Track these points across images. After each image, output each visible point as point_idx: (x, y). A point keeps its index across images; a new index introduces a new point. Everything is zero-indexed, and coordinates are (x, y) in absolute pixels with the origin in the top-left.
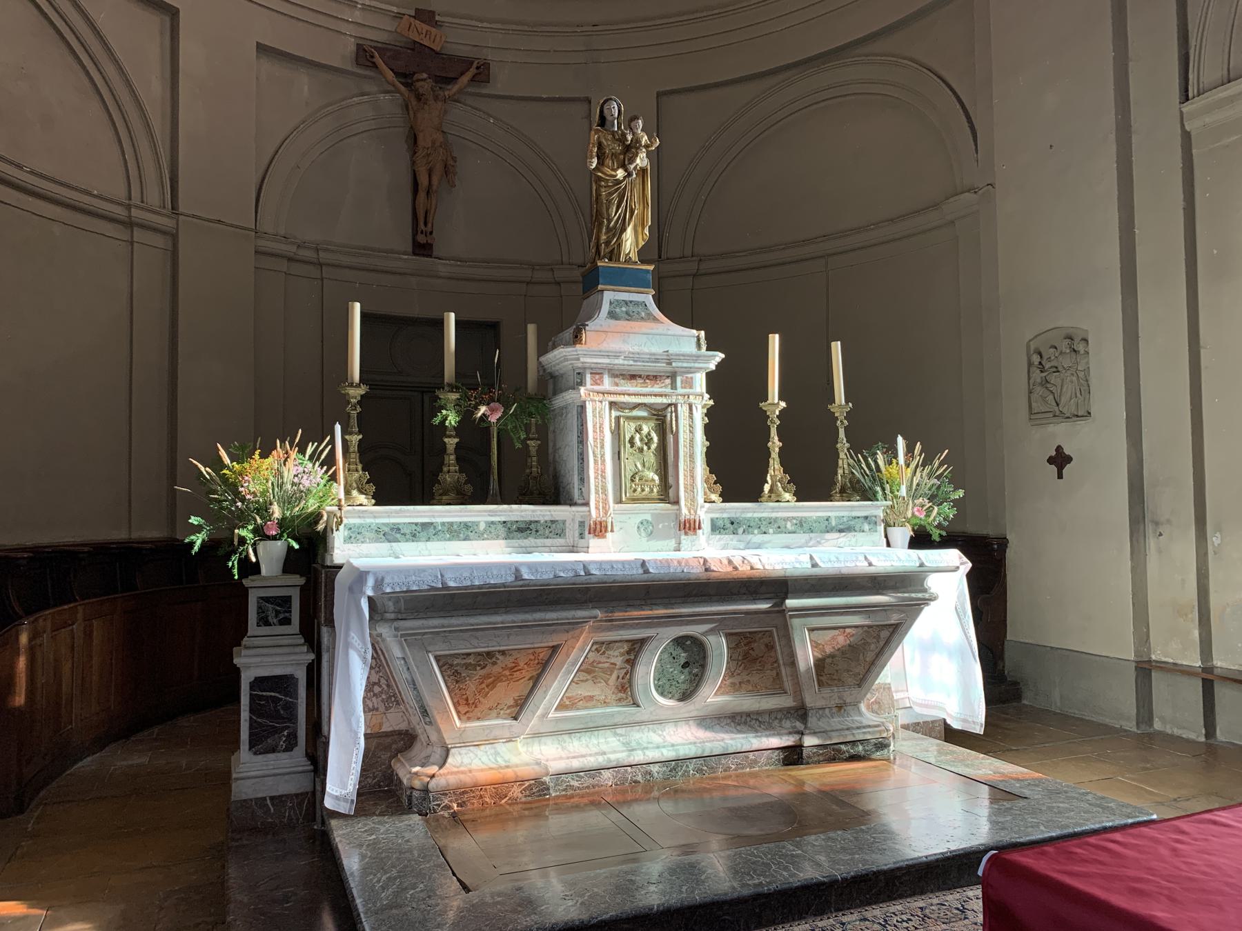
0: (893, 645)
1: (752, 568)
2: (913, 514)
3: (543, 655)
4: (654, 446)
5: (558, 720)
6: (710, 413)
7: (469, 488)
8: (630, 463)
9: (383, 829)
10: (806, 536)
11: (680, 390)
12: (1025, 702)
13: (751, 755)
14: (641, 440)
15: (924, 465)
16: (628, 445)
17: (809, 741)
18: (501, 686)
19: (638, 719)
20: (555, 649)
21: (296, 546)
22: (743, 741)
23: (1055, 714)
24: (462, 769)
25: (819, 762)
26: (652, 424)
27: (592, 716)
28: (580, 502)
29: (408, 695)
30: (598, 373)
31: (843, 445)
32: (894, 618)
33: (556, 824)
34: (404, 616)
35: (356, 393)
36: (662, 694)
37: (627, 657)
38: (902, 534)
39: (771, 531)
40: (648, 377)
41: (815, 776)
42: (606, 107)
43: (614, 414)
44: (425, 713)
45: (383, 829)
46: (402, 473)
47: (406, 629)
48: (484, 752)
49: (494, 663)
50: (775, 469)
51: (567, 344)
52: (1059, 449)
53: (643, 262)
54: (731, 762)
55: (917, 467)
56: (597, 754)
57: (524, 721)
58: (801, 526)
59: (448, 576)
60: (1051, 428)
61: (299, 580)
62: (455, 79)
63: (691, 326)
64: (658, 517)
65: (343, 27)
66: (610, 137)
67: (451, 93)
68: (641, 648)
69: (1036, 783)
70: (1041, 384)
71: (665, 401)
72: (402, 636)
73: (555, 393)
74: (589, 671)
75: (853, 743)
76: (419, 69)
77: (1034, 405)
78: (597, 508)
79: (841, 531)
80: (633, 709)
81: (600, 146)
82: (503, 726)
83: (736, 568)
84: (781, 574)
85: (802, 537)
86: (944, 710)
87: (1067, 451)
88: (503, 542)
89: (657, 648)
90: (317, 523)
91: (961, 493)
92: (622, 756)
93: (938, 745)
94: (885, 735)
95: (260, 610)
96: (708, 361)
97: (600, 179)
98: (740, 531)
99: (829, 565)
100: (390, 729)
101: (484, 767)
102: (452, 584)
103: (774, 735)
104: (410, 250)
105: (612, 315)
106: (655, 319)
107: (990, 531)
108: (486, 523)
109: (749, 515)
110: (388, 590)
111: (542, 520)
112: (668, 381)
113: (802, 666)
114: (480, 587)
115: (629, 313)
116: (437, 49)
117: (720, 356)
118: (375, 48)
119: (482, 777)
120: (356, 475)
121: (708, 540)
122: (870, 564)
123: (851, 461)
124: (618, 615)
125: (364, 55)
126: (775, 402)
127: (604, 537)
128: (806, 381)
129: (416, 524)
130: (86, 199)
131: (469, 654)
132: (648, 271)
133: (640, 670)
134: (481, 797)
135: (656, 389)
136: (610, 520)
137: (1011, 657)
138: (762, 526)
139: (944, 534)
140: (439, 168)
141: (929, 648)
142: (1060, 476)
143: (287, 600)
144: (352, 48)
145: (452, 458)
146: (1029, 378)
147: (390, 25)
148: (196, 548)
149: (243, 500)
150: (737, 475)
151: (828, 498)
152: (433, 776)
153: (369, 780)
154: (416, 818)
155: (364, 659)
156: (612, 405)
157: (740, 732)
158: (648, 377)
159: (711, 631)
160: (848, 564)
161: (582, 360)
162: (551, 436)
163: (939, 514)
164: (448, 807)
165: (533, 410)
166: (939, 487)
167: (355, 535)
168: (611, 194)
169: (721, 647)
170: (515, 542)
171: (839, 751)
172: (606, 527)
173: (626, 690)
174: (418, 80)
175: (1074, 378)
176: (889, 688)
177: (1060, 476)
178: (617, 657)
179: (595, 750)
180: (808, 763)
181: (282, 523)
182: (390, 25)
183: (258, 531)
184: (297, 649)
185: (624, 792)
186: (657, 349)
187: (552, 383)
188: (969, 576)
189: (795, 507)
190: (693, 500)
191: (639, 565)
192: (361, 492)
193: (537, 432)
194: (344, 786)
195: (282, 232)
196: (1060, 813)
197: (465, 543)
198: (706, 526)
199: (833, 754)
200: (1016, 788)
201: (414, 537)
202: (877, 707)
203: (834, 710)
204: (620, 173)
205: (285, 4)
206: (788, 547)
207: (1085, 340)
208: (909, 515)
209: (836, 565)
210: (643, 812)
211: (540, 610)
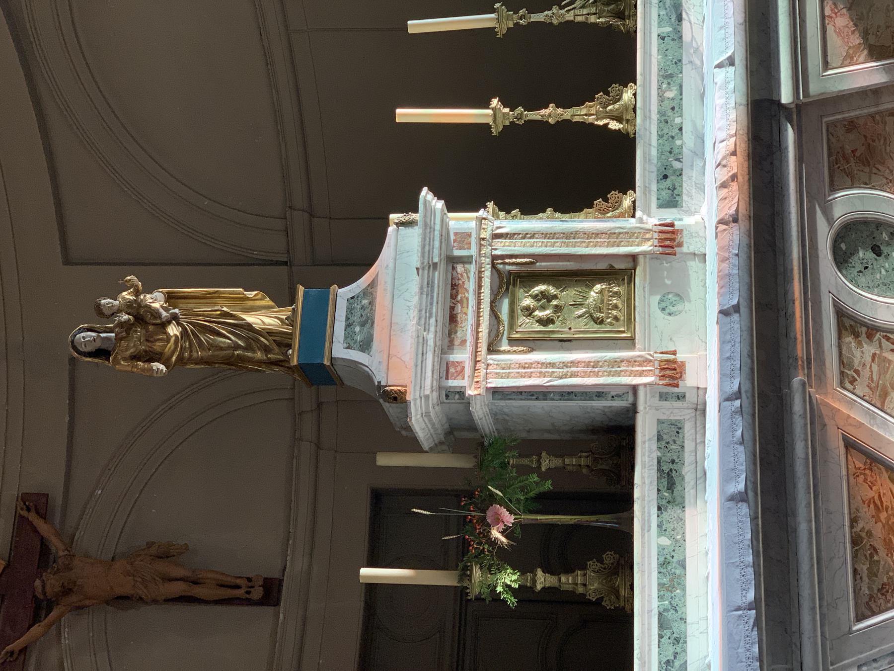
1: (734, 153)
3: (859, 462)
4: (552, 290)
6: (505, 207)
7: (609, 557)
8: (575, 324)
10: (686, 68)
11: (473, 251)
14: (543, 308)
16: (551, 327)
20: (850, 445)
26: (520, 292)
30: (446, 369)
39: (678, 120)
40: (453, 297)
42: (83, 349)
43: (505, 347)
49: (869, 534)
50: (587, 113)
51: (406, 412)
53: (292, 301)
58: (671, 76)
64: (655, 285)
67: (61, 546)
71: (487, 274)
73: (472, 427)
78: (641, 374)
79: (680, 19)
81: (135, 357)
83: (734, 177)
84: (743, 110)
85: (688, 77)
88: (687, 510)
96: (433, 212)
97: (180, 359)
99: (731, 40)
102: (751, 595)
104: (270, 610)
105: (366, 346)
106: (373, 284)
108: (659, 536)
109: (654, 152)
111: (656, 454)
112: (460, 268)
114: (756, 554)
115: (363, 318)
117: (425, 194)
124: (800, 351)
127: (683, 364)
128: (461, 69)
129: (661, 637)
131: (855, 571)
135: (471, 285)
136: (659, 356)
138: (670, 131)
140: (162, 567)
145: (566, 581)
150: (596, 169)
158: (453, 297)
160: (731, 12)
161: (427, 392)
162: (535, 436)
165: (497, 462)
169: (849, 198)
174: (44, 593)
178: (863, 353)
186: (414, 284)
187: (459, 432)
189: (643, 86)
190: (631, 234)
191: (728, 319)
193: (528, 456)
198: (669, 215)
204: (173, 330)
206: (702, 96)
209: (731, 30)
211: (792, 466)
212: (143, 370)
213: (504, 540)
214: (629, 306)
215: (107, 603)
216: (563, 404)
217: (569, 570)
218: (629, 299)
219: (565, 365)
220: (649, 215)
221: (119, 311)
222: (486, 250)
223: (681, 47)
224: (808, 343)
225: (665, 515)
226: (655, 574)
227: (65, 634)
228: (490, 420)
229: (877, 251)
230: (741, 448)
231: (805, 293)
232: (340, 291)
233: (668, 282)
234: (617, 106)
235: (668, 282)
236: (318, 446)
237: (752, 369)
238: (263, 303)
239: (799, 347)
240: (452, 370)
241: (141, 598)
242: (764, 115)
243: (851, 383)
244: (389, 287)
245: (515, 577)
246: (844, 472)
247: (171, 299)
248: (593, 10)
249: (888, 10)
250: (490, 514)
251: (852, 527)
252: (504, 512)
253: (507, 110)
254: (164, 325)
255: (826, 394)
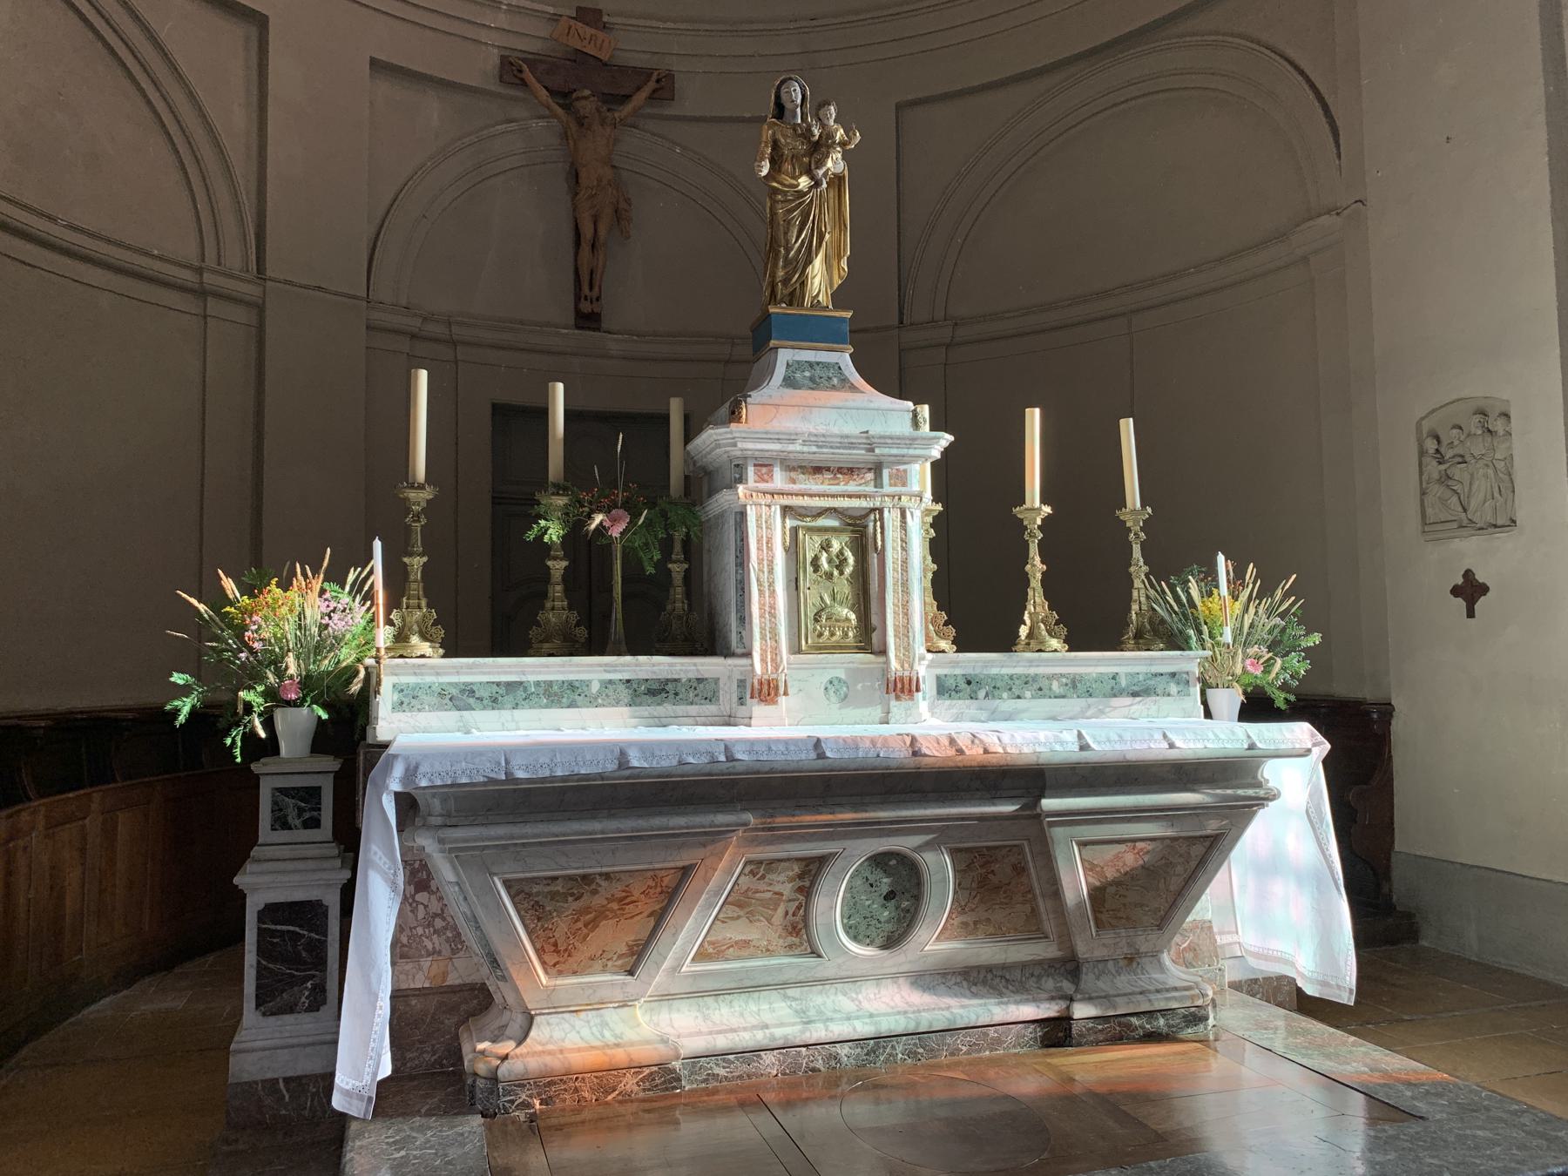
0: (1210, 867)
1: (986, 751)
2: (1244, 670)
4: (848, 570)
5: (696, 976)
7: (582, 632)
9: (421, 1139)
10: (1082, 702)
11: (887, 489)
12: (1424, 943)
13: (991, 1032)
14: (830, 561)
15: (1260, 596)
16: (810, 569)
17: (1081, 1011)
18: (606, 926)
19: (819, 976)
20: (686, 872)
21: (325, 716)
22: (980, 1010)
23: (1470, 962)
24: (550, 1047)
25: (1097, 1043)
26: (846, 538)
27: (747, 970)
28: (739, 651)
29: (469, 935)
30: (765, 464)
31: (1139, 568)
32: (1212, 827)
33: (692, 1130)
34: (454, 821)
35: (420, 498)
36: (855, 938)
37: (799, 883)
38: (1228, 700)
39: (1028, 694)
40: (840, 470)
41: (1092, 1066)
42: (783, 90)
43: (789, 523)
44: (495, 963)
45: (421, 1139)
46: (492, 610)
47: (456, 841)
48: (586, 1023)
49: (595, 892)
50: (1037, 604)
52: (1468, 574)
53: (836, 306)
54: (961, 1042)
55: (1250, 598)
56: (754, 1027)
57: (643, 977)
58: (1075, 687)
59: (516, 762)
60: (1457, 544)
61: (331, 764)
62: (628, 97)
63: (901, 396)
64: (856, 674)
65: (483, 36)
66: (790, 132)
68: (819, 870)
69: (1435, 1091)
70: (1440, 481)
72: (451, 850)
73: (711, 494)
74: (740, 903)
75: (1150, 1014)
76: (582, 85)
77: (1429, 511)
78: (763, 661)
79: (1135, 694)
80: (813, 961)
81: (776, 145)
82: (612, 984)
83: (960, 752)
84: (1032, 760)
85: (1074, 704)
86: (1293, 965)
87: (1481, 577)
88: (626, 710)
89: (845, 870)
90: (349, 682)
91: (1316, 639)
92: (792, 1031)
93: (1286, 1017)
94: (1199, 1003)
95: (277, 808)
96: (928, 446)
97: (775, 191)
98: (982, 694)
99: (1107, 747)
100: (457, 982)
101: (583, 1045)
102: (521, 774)
103: (1027, 1001)
104: (572, 322)
105: (789, 382)
106: (853, 388)
107: (1367, 693)
109: (994, 671)
110: (424, 783)
112: (870, 476)
113: (1070, 897)
114: (564, 779)
115: (820, 379)
116: (604, 56)
117: (946, 439)
118: (524, 60)
119: (577, 1060)
120: (418, 614)
121: (931, 709)
122: (1172, 746)
123: (1152, 592)
124: (781, 820)
125: (511, 70)
126: (1035, 506)
127: (774, 702)
128: (1082, 476)
129: (498, 684)
130: (158, 266)
131: (555, 878)
132: (843, 319)
133: (820, 903)
134: (576, 1090)
135: (852, 487)
137: (1401, 882)
138: (1015, 687)
139: (1292, 698)
141: (1269, 868)
142: (1471, 614)
143: (313, 794)
144: (494, 59)
145: (557, 590)
146: (1421, 473)
147: (544, 30)
148: (182, 718)
149: (251, 650)
150: (977, 609)
151: (1115, 644)
152: (505, 1058)
153: (426, 1056)
154: (477, 1121)
155: (394, 888)
156: (786, 510)
157: (975, 995)
158: (840, 470)
159: (927, 846)
160: (1137, 746)
163: (1284, 669)
164: (526, 1105)
166: (1283, 630)
167: (408, 699)
168: (791, 211)
170: (645, 711)
171: (1129, 1026)
172: (777, 688)
173: (799, 931)
174: (578, 99)
175: (1490, 472)
176: (1210, 928)
177: (1471, 614)
179: (753, 1021)
180: (1079, 1045)
181: (308, 683)
182: (544, 30)
183: (270, 694)
184: (327, 864)
185: (795, 1086)
186: (852, 428)
187: (705, 481)
188: (1327, 762)
189: (1063, 659)
190: (908, 648)
191: (810, 747)
192: (424, 637)
194: (359, 1077)
195: (404, 302)
196: (1477, 1148)
197: (572, 714)
198: (928, 686)
199: (1118, 1031)
200: (1405, 1099)
201: (494, 702)
202: (1190, 958)
203: (1122, 963)
204: (804, 182)
205: (399, 4)
206: (1054, 718)
207: (1506, 415)
208: (1238, 671)
209: (1118, 747)
210: (820, 1116)
211: (661, 814)
212: (763, 154)
213: (593, 526)
214: (834, 647)
215: (572, 164)
216: (733, 582)
217: (566, 591)
218: (841, 648)
219: (771, 584)
220: (929, 666)
221: (823, 126)
222: (888, 502)
223: (1105, 696)
224: (791, 828)
225: (622, 687)
226: (560, 677)
227: (542, 123)
228: (717, 511)
229: (890, 896)
230: (675, 763)
231: (842, 825)
232: (847, 356)
233: (859, 686)
234: (1044, 633)
235: (859, 686)
236: (727, 362)
237: (758, 772)
238: (836, 277)
239: (785, 819)
240: (764, 470)
241: (577, 194)
242: (1030, 781)
243: (751, 872)
244: (850, 404)
245: (554, 538)
246: (657, 866)
247: (837, 181)
248: (1144, 607)
249: (1142, 905)
250: (621, 512)
251: (601, 874)
252: (621, 527)
253: (1039, 522)
254: (809, 172)
255: (738, 846)
